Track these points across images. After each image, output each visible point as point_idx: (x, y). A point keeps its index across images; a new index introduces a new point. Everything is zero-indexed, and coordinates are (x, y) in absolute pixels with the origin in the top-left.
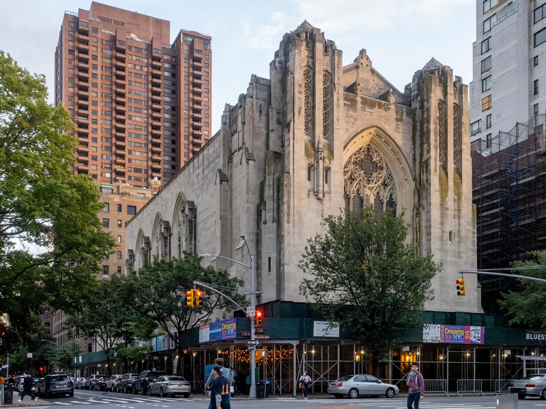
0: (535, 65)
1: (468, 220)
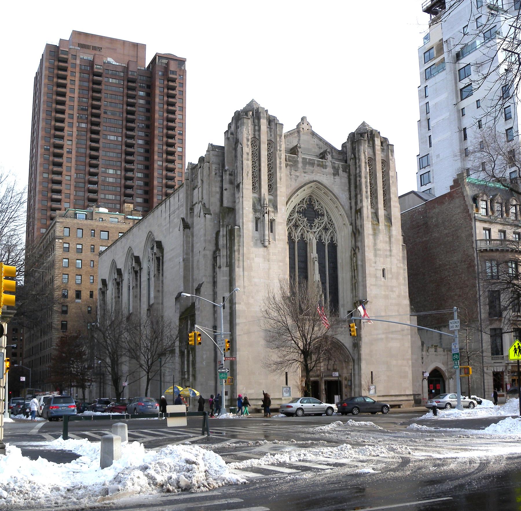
0: (463, 115)
1: (398, 258)
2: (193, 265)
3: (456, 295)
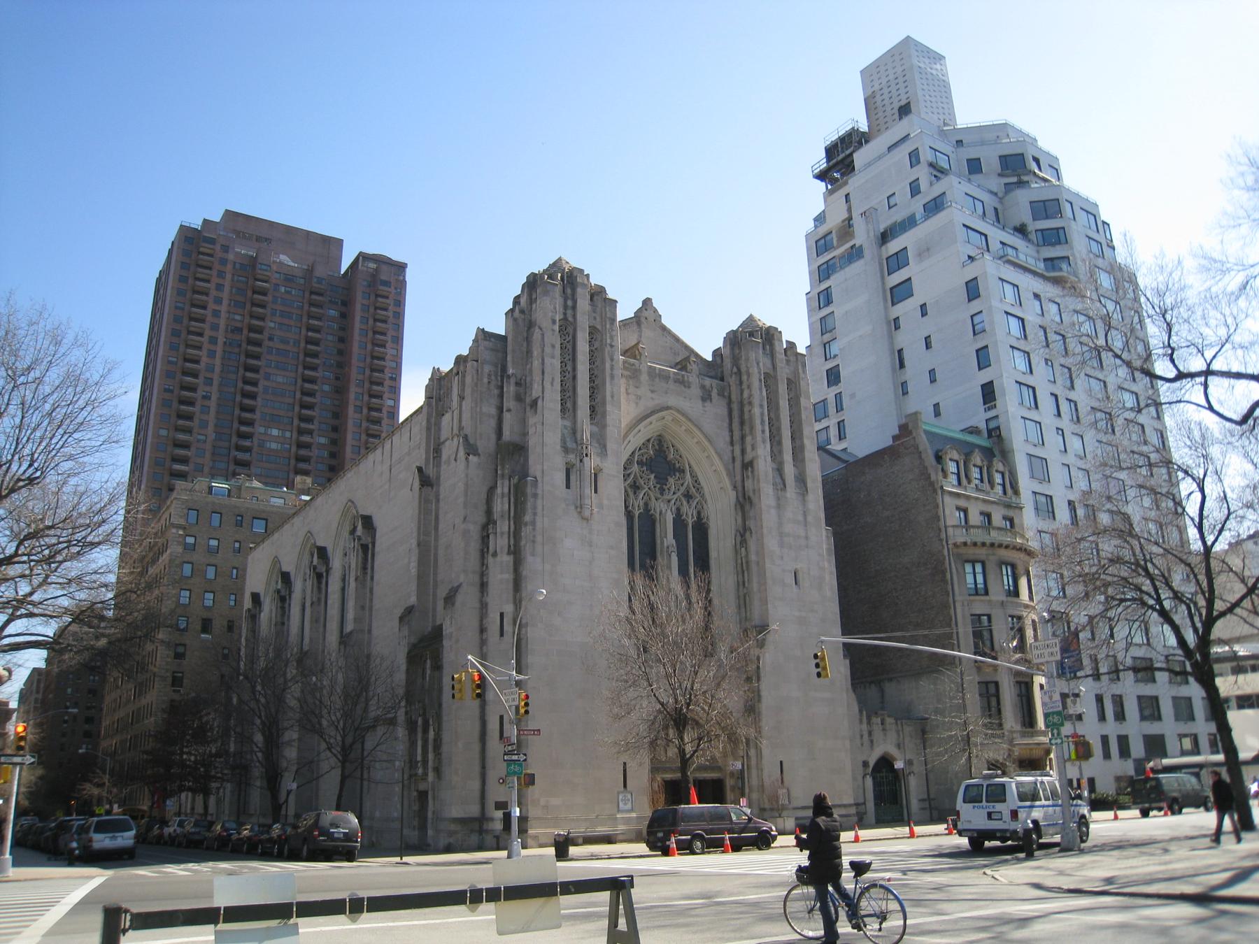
2: (436, 555)
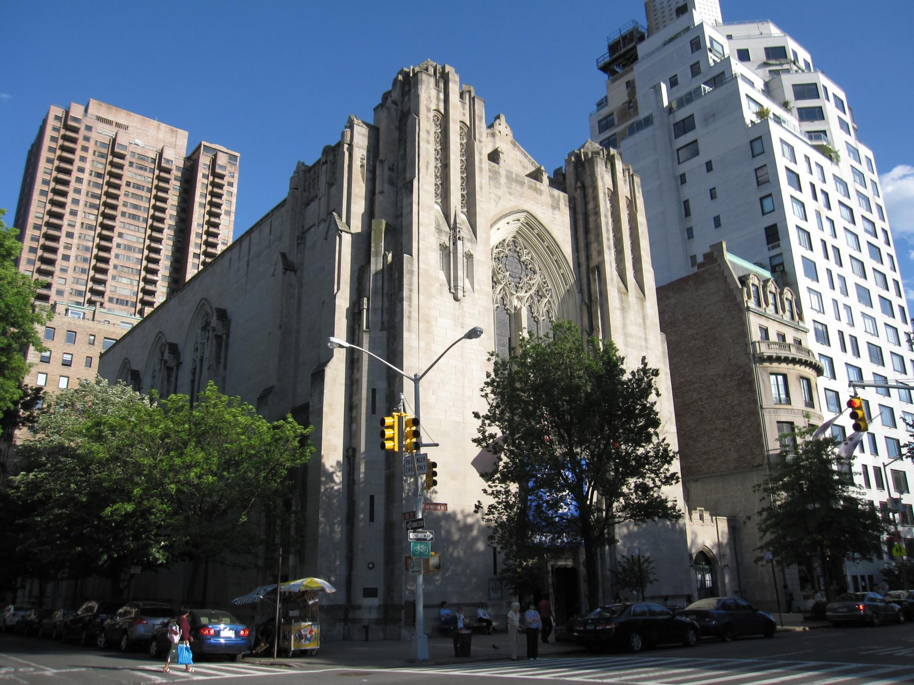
3: (716, 429)
